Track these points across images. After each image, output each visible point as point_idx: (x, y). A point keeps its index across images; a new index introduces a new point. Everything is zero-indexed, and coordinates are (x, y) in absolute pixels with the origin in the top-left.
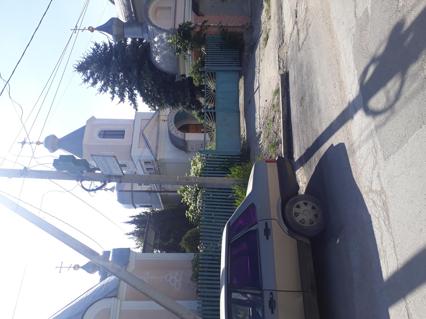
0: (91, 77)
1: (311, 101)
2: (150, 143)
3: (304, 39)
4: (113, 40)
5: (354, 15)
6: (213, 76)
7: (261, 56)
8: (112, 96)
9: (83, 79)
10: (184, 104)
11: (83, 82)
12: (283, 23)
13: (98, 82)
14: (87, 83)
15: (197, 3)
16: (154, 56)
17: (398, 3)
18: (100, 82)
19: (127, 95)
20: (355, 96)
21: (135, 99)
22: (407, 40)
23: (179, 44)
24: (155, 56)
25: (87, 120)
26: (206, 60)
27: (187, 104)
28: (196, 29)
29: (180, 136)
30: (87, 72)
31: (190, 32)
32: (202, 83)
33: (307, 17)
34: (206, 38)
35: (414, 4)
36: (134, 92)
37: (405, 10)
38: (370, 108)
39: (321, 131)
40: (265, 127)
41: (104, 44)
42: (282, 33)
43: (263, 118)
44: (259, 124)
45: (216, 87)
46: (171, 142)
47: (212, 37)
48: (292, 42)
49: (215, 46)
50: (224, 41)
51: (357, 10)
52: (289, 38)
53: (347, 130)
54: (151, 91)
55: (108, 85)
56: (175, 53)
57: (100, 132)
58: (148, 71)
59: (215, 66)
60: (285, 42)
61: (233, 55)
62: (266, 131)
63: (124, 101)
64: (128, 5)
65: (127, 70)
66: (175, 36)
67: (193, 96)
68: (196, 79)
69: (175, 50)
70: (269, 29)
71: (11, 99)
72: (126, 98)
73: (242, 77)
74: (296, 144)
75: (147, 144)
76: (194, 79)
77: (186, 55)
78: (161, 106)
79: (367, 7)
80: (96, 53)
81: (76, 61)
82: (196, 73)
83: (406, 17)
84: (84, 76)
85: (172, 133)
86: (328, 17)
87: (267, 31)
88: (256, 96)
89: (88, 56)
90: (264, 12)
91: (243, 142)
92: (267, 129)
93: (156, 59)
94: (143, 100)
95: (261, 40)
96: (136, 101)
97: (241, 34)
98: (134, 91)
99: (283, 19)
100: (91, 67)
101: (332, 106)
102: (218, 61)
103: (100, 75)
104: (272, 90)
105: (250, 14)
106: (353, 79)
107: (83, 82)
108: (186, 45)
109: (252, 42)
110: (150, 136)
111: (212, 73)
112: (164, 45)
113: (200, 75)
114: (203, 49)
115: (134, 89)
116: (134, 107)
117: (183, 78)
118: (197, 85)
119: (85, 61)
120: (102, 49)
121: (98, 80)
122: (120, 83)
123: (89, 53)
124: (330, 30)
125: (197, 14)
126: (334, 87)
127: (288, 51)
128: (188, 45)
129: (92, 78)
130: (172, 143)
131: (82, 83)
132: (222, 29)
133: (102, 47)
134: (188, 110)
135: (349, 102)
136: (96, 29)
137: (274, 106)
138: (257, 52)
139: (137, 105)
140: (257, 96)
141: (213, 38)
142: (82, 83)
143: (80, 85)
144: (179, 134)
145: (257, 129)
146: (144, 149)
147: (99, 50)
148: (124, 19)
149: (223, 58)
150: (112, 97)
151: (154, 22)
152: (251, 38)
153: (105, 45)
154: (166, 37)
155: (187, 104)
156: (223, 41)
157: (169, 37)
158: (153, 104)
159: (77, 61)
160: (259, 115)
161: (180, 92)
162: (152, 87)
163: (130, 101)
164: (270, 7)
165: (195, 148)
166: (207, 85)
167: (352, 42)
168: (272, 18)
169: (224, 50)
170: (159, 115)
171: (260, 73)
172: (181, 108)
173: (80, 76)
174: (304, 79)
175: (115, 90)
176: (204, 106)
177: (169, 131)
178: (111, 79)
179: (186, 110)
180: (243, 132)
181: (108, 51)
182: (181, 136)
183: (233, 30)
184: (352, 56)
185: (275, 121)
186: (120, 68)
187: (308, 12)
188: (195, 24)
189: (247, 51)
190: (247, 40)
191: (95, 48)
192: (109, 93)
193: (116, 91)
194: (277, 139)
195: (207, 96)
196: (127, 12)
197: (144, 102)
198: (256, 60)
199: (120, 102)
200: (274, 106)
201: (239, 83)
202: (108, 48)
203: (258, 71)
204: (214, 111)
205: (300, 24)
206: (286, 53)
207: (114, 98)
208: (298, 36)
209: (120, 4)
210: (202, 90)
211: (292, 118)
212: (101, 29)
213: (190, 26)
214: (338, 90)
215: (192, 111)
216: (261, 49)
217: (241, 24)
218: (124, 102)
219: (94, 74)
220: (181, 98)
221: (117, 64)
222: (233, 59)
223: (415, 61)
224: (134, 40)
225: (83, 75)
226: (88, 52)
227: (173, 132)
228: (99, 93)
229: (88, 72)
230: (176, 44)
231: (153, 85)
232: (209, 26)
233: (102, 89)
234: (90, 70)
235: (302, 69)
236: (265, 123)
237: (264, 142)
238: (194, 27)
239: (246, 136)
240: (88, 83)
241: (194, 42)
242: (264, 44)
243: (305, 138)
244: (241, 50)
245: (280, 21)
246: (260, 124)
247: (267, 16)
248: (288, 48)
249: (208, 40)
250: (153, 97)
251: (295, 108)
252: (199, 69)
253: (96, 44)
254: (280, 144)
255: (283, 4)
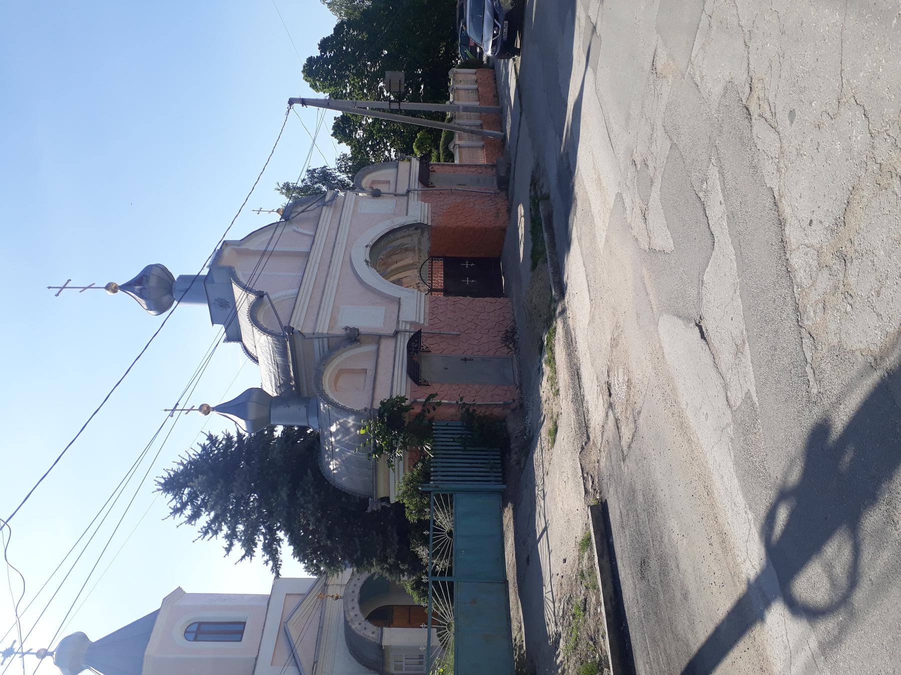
0: (189, 503)
1: (664, 571)
2: (300, 652)
3: (631, 438)
4: (245, 429)
5: (726, 403)
6: (446, 501)
7: (546, 464)
8: (228, 545)
9: (173, 507)
10: (383, 560)
11: (171, 513)
12: (584, 405)
13: (203, 513)
14: (178, 515)
15: (417, 362)
16: (327, 460)
17: (809, 387)
18: (207, 513)
19: (260, 541)
20: (758, 569)
21: (277, 549)
22: (843, 459)
23: (378, 437)
24: (330, 460)
25: (163, 598)
26: (432, 469)
27: (391, 561)
28: (413, 409)
29: (371, 635)
30: (183, 494)
31: (402, 415)
32: (424, 516)
33: (631, 397)
34: (433, 426)
35: (840, 393)
36: (276, 534)
37: (826, 402)
38: (799, 601)
39: (695, 644)
40: (567, 622)
41: (226, 437)
42: (584, 422)
43: (560, 600)
44: (552, 614)
45: (455, 524)
46: (348, 651)
47: (445, 424)
48: (607, 442)
49: (452, 442)
50: (469, 432)
51: (729, 394)
52: (600, 434)
53: (756, 648)
54: (313, 533)
55: (223, 520)
56: (370, 455)
57: (188, 627)
58: (311, 490)
59: (452, 481)
60: (591, 440)
61: (487, 459)
62: (571, 633)
63: (253, 556)
64: (285, 366)
65: (267, 490)
66: (371, 422)
67: (405, 542)
68: (412, 507)
69: (370, 448)
70: (557, 414)
71: (6, 560)
72: (259, 550)
73: (508, 504)
74: (644, 671)
75: (292, 655)
76: (408, 508)
77: (392, 458)
78: (334, 565)
79: (749, 390)
80: (208, 454)
81: (164, 469)
82: (412, 496)
83: (831, 415)
84: (174, 500)
85: (353, 627)
86: (673, 402)
87: (554, 417)
88: (542, 547)
89: (191, 459)
90: (546, 381)
91: (518, 656)
92: (573, 628)
93: (331, 467)
94: (294, 552)
95: (544, 432)
96: (279, 554)
97: (504, 420)
98: (278, 532)
99: (584, 397)
100: (193, 482)
101: (711, 585)
102: (458, 472)
103: (208, 499)
104: (576, 537)
105: (517, 384)
106: (748, 531)
107: (170, 515)
108: (394, 439)
109: (526, 435)
110: (301, 636)
111: (445, 496)
112: (349, 439)
113: (421, 498)
114: (427, 447)
115: (278, 529)
116: (272, 569)
117: (384, 504)
118: (413, 520)
119: (182, 470)
120: (222, 447)
121: (204, 509)
122: (249, 515)
123: (194, 454)
124: (683, 427)
125: (416, 383)
126: (708, 544)
127: (601, 459)
128: (398, 440)
129: (192, 504)
130: (350, 652)
131: (168, 517)
132: (464, 409)
133: (221, 443)
134: (391, 573)
135: (748, 580)
136: (214, 409)
137: (582, 576)
138: (537, 455)
139: (279, 563)
140: (544, 548)
141: (447, 425)
142: (168, 517)
143: (163, 520)
144: (369, 631)
145: (548, 625)
146: (264, 260)
147: (215, 449)
148: (274, 391)
149: (467, 465)
150: (227, 546)
151: (331, 396)
152: (523, 427)
153: (229, 438)
154: (354, 425)
155: (389, 561)
156: (467, 432)
157: (359, 424)
158: (315, 561)
159: (167, 470)
160: (551, 593)
161: (375, 534)
162: (317, 523)
163: (266, 555)
164: (556, 373)
165: (404, 666)
166: (435, 521)
167: (732, 454)
168: (562, 392)
169: (469, 448)
170: (325, 585)
171: (547, 498)
172: (376, 569)
173: (167, 501)
174: (641, 521)
175: (237, 530)
176: (427, 565)
177: (346, 622)
178: (231, 507)
179: (387, 575)
180: (518, 633)
181: (233, 449)
182: (374, 636)
183: (486, 412)
184: (736, 481)
185: (588, 610)
186: (253, 484)
187: (632, 389)
188: (413, 400)
189: (516, 453)
190: (515, 431)
191: (208, 445)
192: (223, 537)
193: (238, 533)
194: (598, 654)
195: (435, 546)
196: (282, 379)
197: (295, 558)
198: (536, 472)
199: (243, 557)
200: (582, 576)
201: (504, 518)
202: (233, 444)
203: (541, 493)
204: (447, 579)
205: (619, 409)
206: (598, 462)
207: (233, 548)
208: (617, 430)
209: (269, 364)
210: (424, 533)
211: (626, 606)
212: (224, 408)
213: (403, 404)
214: (719, 552)
215: (401, 576)
216: (544, 450)
217: (501, 401)
218: (253, 557)
219: (198, 496)
220: (378, 547)
221: (248, 476)
222: (487, 468)
223: (872, 504)
224: (288, 430)
225: (173, 499)
226: (191, 452)
227: (354, 624)
228: (202, 537)
229: (185, 493)
230: (374, 438)
231: (318, 520)
232: (439, 404)
233: (208, 529)
234: (189, 489)
235: (634, 497)
236: (566, 614)
237: (568, 661)
238: (410, 406)
239: (524, 642)
240: (180, 515)
241: (410, 433)
242: (550, 440)
243: (662, 659)
244: (505, 450)
245: (579, 399)
246: (554, 615)
247: (552, 389)
248: (599, 451)
249: (437, 430)
250: (317, 545)
251: (631, 582)
252: (418, 487)
253: (210, 437)
254: (606, 669)
255: (582, 369)
